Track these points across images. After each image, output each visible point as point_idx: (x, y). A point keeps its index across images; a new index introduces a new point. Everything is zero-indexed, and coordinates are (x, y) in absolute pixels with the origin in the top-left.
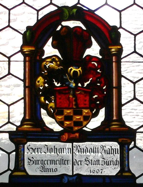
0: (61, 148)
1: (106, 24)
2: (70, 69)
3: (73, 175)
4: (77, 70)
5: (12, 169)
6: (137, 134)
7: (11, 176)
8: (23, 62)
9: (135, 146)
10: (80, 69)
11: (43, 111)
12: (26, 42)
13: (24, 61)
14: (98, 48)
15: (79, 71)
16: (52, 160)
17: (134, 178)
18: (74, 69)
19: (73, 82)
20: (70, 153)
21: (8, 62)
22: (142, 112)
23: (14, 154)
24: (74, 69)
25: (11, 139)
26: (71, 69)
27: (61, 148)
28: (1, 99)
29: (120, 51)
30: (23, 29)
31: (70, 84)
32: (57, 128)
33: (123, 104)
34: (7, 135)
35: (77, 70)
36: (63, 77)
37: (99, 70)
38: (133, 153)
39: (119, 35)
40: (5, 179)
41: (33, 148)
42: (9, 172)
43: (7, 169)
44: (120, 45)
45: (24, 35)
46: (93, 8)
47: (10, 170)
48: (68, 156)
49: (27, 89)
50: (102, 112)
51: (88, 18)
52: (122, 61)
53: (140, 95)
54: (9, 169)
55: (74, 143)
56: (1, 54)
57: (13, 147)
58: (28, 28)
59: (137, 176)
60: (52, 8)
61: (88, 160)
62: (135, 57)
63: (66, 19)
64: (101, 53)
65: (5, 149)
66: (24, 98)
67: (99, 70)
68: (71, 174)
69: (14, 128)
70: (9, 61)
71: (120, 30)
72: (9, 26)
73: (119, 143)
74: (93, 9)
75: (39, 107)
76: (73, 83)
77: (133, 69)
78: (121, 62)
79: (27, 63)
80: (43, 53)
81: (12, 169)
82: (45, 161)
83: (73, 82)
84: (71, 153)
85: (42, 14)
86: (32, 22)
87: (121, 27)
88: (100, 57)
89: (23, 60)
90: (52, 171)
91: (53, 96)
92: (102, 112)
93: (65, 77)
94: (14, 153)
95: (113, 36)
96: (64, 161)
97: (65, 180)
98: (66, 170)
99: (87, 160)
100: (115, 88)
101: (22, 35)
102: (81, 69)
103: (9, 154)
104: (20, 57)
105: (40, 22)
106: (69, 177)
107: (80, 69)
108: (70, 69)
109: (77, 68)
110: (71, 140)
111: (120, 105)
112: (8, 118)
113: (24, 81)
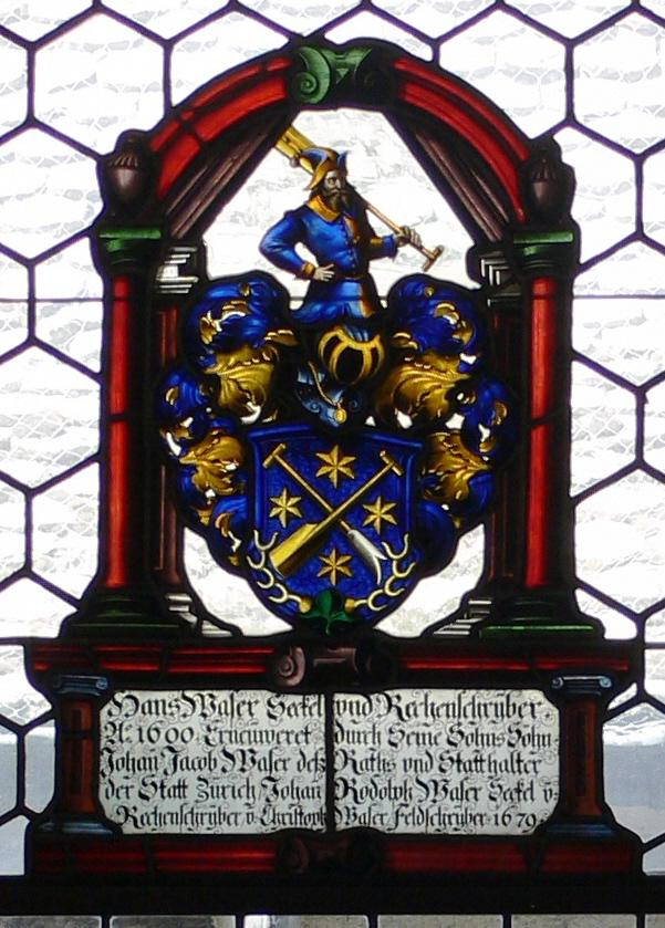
2: (329, 336)
4: (366, 348)
6: (501, 917)
8: (100, 305)
9: (642, 697)
10: (376, 343)
11: (195, 551)
13: (103, 300)
15: (374, 351)
18: (347, 342)
19: (336, 399)
20: (316, 716)
21: (26, 305)
24: (347, 342)
25: (37, 678)
26: (335, 341)
28: (4, 243)
29: (575, 246)
35: (366, 348)
36: (297, 377)
39: (564, 182)
43: (13, 806)
44: (574, 228)
50: (471, 549)
51: (413, 95)
54: (20, 809)
55: (339, 697)
57: (39, 704)
58: (131, 142)
60: (242, 43)
62: (639, 266)
63: (315, 100)
66: (102, 457)
69: (45, 617)
71: (573, 149)
72: (570, 44)
73: (552, 696)
76: (336, 408)
79: (119, 308)
83: (336, 399)
85: (196, 69)
86: (148, 115)
89: (100, 295)
91: (270, 334)
92: (471, 549)
93: (302, 380)
94: (48, 731)
95: (539, 189)
102: (381, 341)
105: (182, 118)
107: (376, 343)
108: (323, 344)
109: (366, 335)
110: (323, 683)
111: (560, 509)
112: (23, 530)
113: (102, 377)
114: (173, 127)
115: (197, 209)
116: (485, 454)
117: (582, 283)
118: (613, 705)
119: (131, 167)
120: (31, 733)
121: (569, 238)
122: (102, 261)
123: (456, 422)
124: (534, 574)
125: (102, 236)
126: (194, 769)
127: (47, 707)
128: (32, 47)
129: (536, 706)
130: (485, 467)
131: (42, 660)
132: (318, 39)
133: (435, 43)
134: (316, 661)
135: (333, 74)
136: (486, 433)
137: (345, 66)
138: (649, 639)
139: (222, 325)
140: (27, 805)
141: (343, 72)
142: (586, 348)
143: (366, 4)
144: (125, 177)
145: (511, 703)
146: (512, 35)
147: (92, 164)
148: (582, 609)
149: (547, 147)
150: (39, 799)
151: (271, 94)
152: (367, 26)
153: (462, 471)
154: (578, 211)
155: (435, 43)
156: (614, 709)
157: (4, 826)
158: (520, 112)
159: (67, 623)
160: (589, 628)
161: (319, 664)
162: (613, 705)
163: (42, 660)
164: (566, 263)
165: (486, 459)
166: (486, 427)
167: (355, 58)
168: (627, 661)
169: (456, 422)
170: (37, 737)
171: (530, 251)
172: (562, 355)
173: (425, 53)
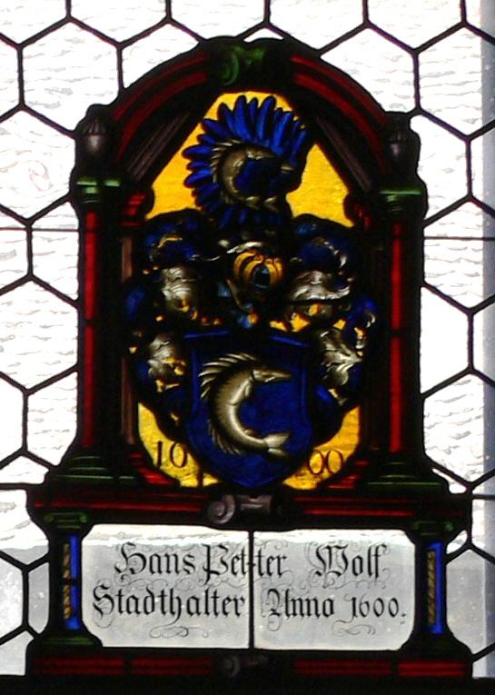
0: (326, 616)
5: (39, 630)
7: (32, 652)
8: (76, 236)
9: (469, 545)
11: (145, 415)
12: (85, 166)
14: (339, 191)
16: (300, 600)
20: (240, 574)
29: (422, 200)
30: (72, 116)
33: (196, 43)
34: (20, 497)
37: (231, 107)
39: (413, 143)
40: (11, 661)
41: (145, 554)
42: (26, 638)
44: (422, 186)
45: (79, 135)
46: (317, 44)
47: (32, 632)
48: (240, 588)
50: (352, 420)
51: (302, 80)
52: (428, 231)
54: (25, 627)
56: (3, 212)
58: (95, 112)
60: (173, 45)
61: (108, 592)
64: (350, 206)
65: (410, 592)
69: (37, 475)
70: (29, 231)
71: (418, 124)
74: (428, 280)
75: (126, 398)
77: (440, 194)
78: (424, 238)
79: (90, 237)
80: (150, 199)
81: (39, 630)
82: (227, 602)
84: (244, 573)
85: (140, 63)
86: (108, 95)
87: (418, 110)
90: (276, 572)
92: (352, 420)
96: (219, 602)
98: (222, 634)
99: (100, 595)
101: (72, 137)
103: (26, 569)
104: (67, 216)
111: (414, 401)
115: (146, 160)
118: (280, 38)
123: (340, 325)
124: (395, 445)
125: (79, 183)
126: (138, 612)
127: (56, 461)
128: (20, 47)
129: (282, 560)
131: (42, 503)
133: (471, 312)
135: (242, 64)
136: (360, 334)
140: (28, 563)
141: (249, 63)
144: (94, 141)
145: (247, 575)
148: (428, 453)
154: (424, 172)
156: (281, 35)
158: (377, 93)
159: (47, 476)
161: (236, 189)
162: (280, 38)
165: (360, 354)
166: (360, 329)
167: (259, 54)
168: (460, 513)
169: (340, 325)
171: (391, 199)
172: (414, 279)
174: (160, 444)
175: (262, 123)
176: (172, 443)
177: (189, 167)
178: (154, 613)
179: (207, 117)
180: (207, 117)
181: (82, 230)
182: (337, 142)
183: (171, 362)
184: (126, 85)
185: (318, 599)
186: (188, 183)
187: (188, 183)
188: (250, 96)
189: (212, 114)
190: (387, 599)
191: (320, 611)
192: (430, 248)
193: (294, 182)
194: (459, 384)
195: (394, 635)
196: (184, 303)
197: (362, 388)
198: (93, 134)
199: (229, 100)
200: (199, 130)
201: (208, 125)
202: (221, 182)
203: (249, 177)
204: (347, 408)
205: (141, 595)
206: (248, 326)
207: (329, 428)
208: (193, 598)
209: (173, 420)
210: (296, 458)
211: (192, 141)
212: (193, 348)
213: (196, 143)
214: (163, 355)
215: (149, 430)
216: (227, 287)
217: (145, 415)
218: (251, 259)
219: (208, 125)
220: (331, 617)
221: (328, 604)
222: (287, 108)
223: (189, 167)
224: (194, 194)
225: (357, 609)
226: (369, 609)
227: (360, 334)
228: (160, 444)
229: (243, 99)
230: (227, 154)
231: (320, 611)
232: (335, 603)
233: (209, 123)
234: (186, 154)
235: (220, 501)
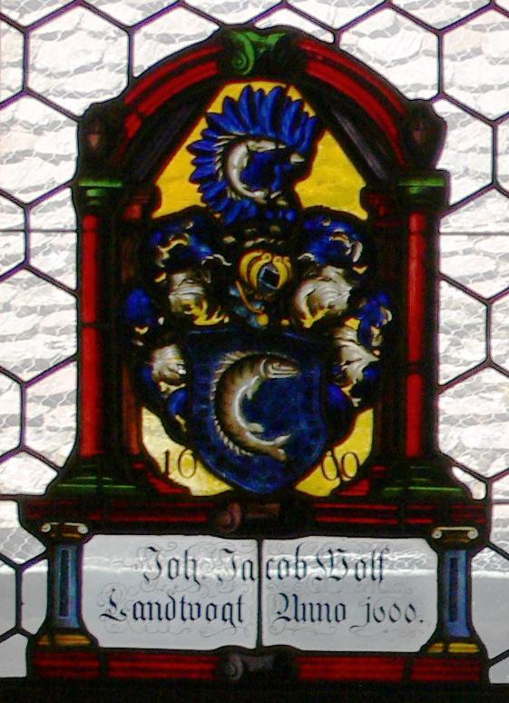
0: (168, 619)
1: (318, 656)
3: (260, 649)
5: (34, 631)
11: (150, 421)
12: (89, 162)
17: (481, 661)
22: (502, 418)
23: (39, 574)
27: (168, 619)
29: (444, 191)
30: (78, 107)
31: (249, 317)
32: (200, 482)
34: (9, 511)
38: (484, 567)
40: (9, 662)
47: (24, 633)
49: (414, 355)
53: (20, 330)
54: (18, 629)
59: (491, 655)
60: (186, 30)
64: (366, 198)
67: (359, 400)
68: (250, 644)
69: (34, 479)
71: (441, 108)
75: (128, 399)
80: (155, 198)
85: (149, 53)
86: (110, 85)
88: (362, 215)
94: (42, 567)
95: (417, 136)
97: (236, 666)
100: (446, 649)
104: (64, 214)
106: (248, 659)
110: (258, 530)
111: (431, 389)
114: (412, 446)
116: (376, 348)
117: (450, 223)
119: (99, 133)
120: (28, 571)
121: (440, 184)
122: (79, 200)
130: (376, 359)
131: (32, 511)
132: (248, 26)
134: (250, 516)
135: (256, 53)
136: (376, 331)
137: (266, 45)
138: (496, 497)
139: (169, 252)
142: (431, 58)
143: (284, 4)
145: (257, 581)
146: (402, 61)
147: (493, 540)
149: (422, 110)
150: (33, 623)
151: (210, 70)
152: (283, 18)
153: (357, 358)
155: (337, 33)
157: (3, 643)
159: (51, 486)
160: (457, 490)
163: (32, 511)
164: (437, 203)
165: (377, 353)
167: (272, 40)
170: (31, 574)
171: (414, 191)
172: (431, 276)
173: (328, 38)
174: (167, 453)
175: (411, 314)
176: (182, 448)
177: (193, 163)
178: (199, 620)
179: (210, 110)
180: (210, 110)
181: (80, 230)
182: (348, 127)
183: (313, 443)
184: (443, 284)
185: (329, 604)
186: (193, 179)
187: (193, 179)
188: (256, 86)
189: (216, 107)
190: (404, 607)
191: (163, 615)
192: (446, 244)
193: (304, 171)
194: (475, 361)
195: (412, 637)
196: (192, 306)
197: (375, 388)
198: (94, 133)
199: (234, 90)
200: (203, 125)
201: (212, 120)
202: (227, 177)
203: (257, 171)
204: (362, 408)
205: (164, 601)
206: (234, 310)
207: (342, 429)
208: (212, 604)
209: (177, 422)
210: (304, 459)
211: (195, 136)
212: (199, 347)
213: (199, 138)
214: (168, 360)
215: (155, 439)
216: (235, 288)
217: (150, 421)
218: (258, 258)
219: (212, 120)
220: (343, 622)
221: (340, 608)
222: (312, 114)
223: (193, 163)
224: (199, 190)
225: (371, 616)
226: (390, 613)
227: (376, 331)
228: (167, 453)
229: (249, 89)
230: (229, 148)
231: (163, 615)
232: (347, 608)
233: (213, 117)
234: (191, 149)
235: (226, 510)
